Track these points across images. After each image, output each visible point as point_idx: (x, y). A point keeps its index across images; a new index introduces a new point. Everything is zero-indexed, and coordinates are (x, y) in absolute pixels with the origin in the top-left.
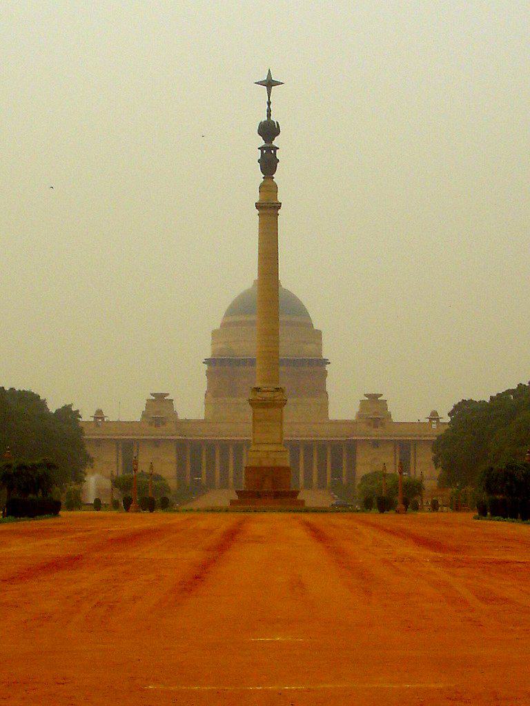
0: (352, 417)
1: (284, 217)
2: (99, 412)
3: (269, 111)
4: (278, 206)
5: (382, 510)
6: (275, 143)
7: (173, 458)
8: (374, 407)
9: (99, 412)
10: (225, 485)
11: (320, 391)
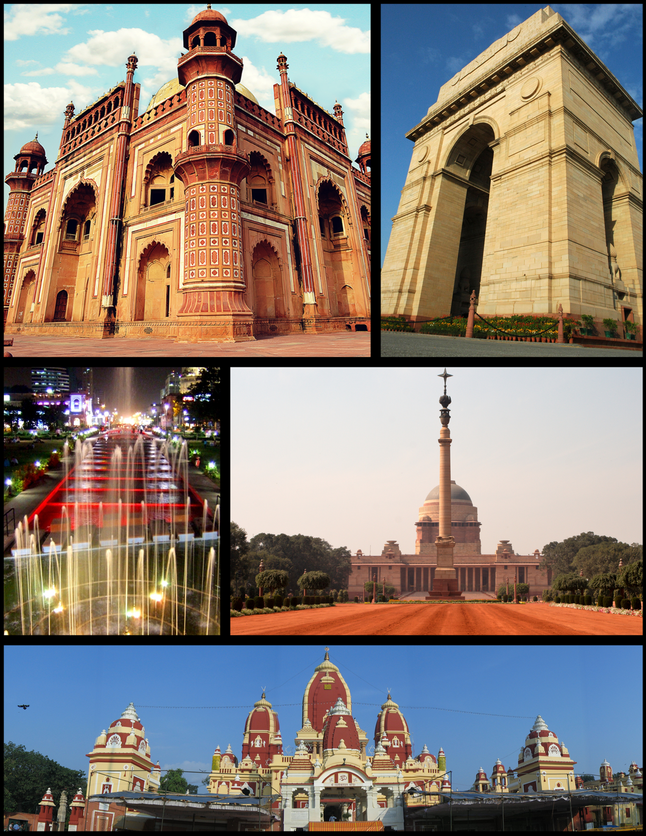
0: (380, 554)
1: (453, 447)
2: (360, 551)
3: (445, 390)
4: (450, 441)
5: (505, 601)
6: (449, 407)
7: (399, 575)
8: (505, 548)
9: (360, 551)
10: (426, 589)
11: (476, 539)
